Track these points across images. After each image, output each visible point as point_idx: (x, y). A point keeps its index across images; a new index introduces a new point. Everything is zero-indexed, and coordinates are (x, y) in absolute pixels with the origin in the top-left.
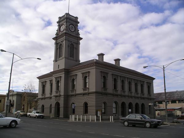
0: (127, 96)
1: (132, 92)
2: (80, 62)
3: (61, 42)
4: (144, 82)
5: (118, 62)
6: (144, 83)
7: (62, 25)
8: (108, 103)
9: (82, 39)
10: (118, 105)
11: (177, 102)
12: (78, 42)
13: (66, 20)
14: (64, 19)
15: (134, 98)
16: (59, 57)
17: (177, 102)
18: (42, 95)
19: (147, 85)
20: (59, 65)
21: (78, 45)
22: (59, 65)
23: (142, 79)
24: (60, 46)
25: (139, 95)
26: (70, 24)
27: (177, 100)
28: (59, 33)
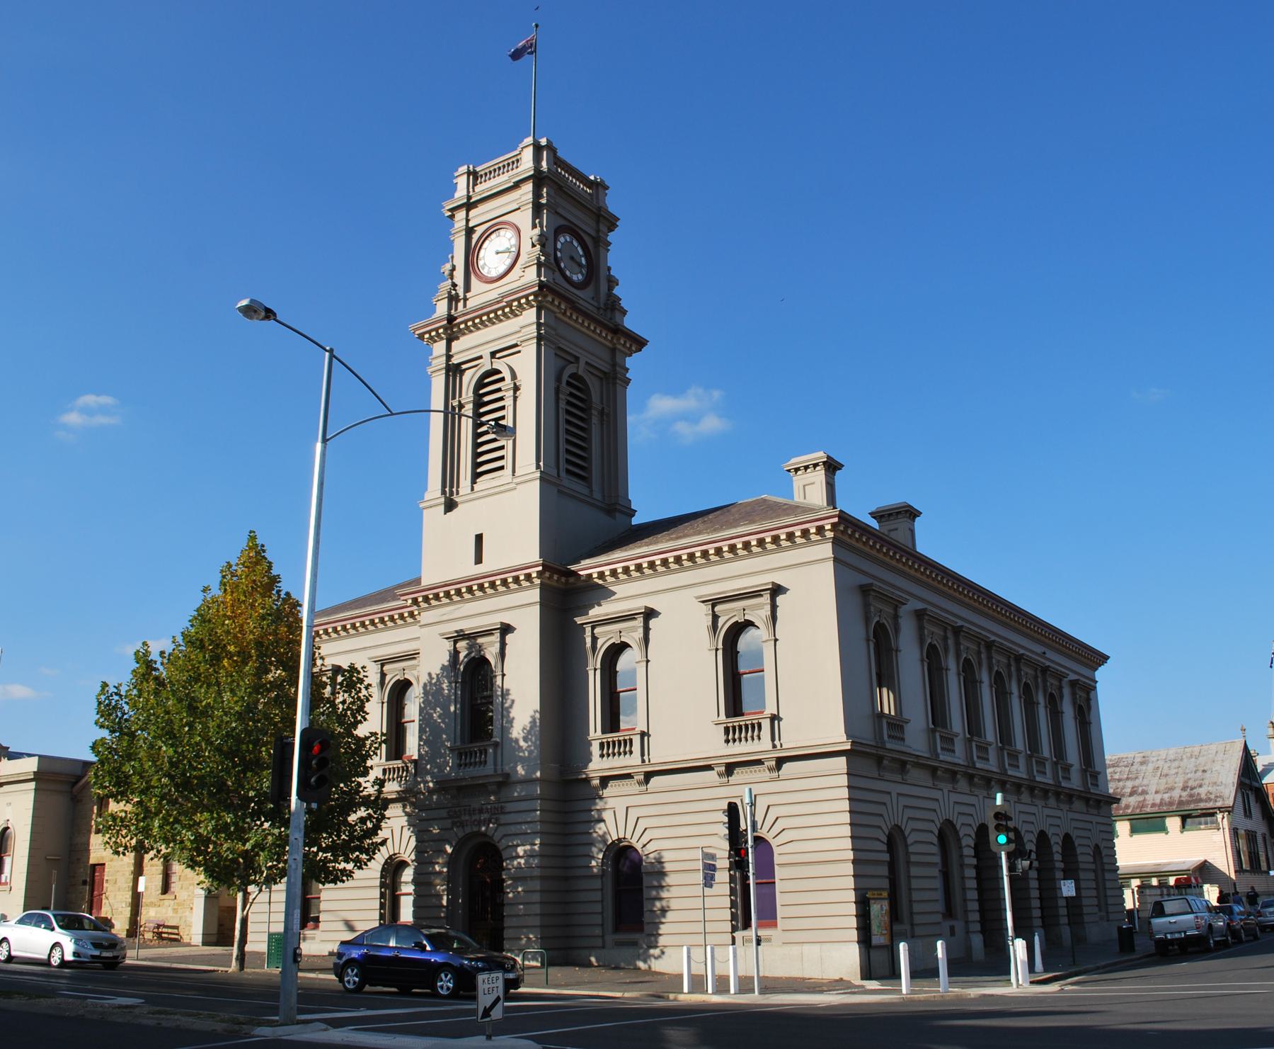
0: (918, 765)
1: (1071, 766)
2: (636, 521)
3: (493, 354)
4: (897, 604)
5: (902, 523)
6: (896, 617)
7: (494, 227)
8: (912, 825)
9: (640, 343)
10: (959, 840)
11: (1173, 823)
12: (614, 365)
13: (537, 194)
14: (517, 185)
15: (1078, 805)
16: (476, 476)
17: (1173, 823)
18: (463, 755)
19: (867, 620)
20: (479, 538)
21: (619, 388)
22: (479, 538)
23: (1031, 648)
24: (480, 384)
25: (959, 756)
26: (563, 222)
27: (1171, 813)
28: (467, 288)
